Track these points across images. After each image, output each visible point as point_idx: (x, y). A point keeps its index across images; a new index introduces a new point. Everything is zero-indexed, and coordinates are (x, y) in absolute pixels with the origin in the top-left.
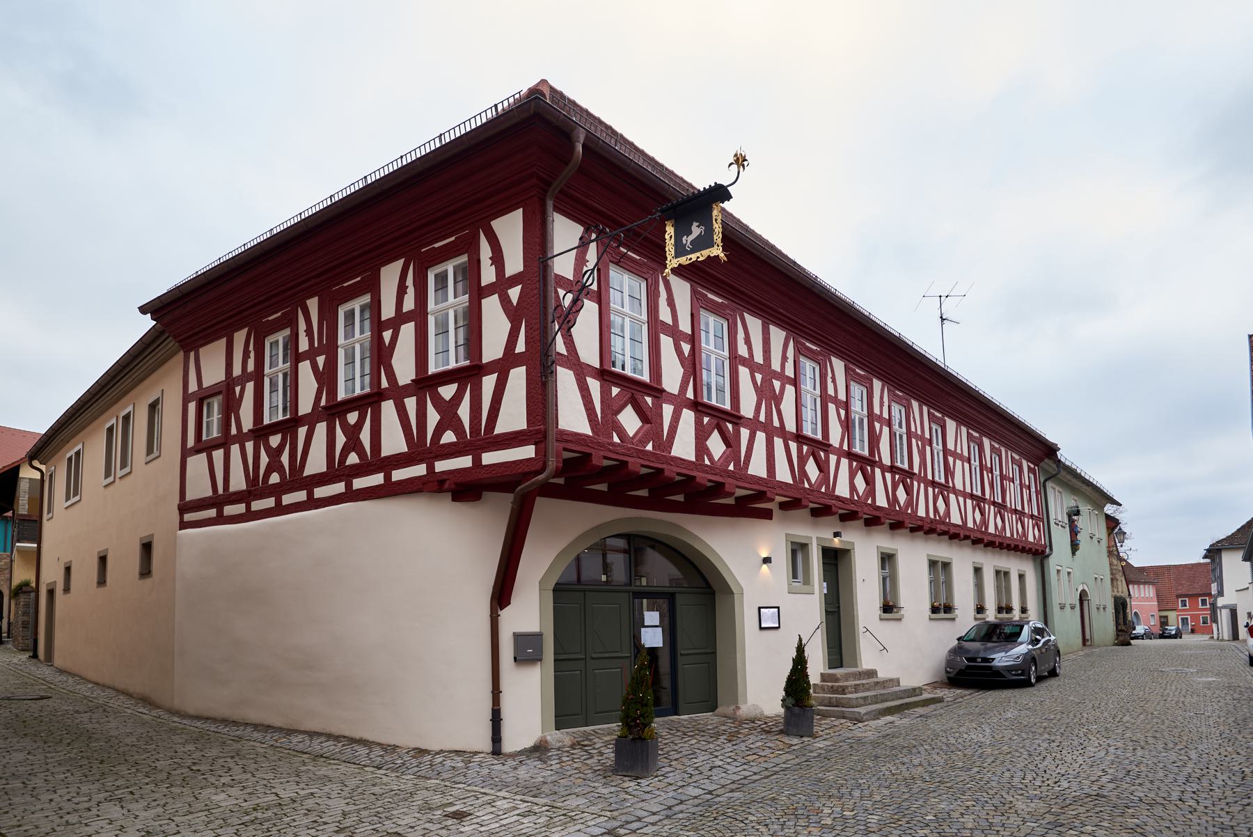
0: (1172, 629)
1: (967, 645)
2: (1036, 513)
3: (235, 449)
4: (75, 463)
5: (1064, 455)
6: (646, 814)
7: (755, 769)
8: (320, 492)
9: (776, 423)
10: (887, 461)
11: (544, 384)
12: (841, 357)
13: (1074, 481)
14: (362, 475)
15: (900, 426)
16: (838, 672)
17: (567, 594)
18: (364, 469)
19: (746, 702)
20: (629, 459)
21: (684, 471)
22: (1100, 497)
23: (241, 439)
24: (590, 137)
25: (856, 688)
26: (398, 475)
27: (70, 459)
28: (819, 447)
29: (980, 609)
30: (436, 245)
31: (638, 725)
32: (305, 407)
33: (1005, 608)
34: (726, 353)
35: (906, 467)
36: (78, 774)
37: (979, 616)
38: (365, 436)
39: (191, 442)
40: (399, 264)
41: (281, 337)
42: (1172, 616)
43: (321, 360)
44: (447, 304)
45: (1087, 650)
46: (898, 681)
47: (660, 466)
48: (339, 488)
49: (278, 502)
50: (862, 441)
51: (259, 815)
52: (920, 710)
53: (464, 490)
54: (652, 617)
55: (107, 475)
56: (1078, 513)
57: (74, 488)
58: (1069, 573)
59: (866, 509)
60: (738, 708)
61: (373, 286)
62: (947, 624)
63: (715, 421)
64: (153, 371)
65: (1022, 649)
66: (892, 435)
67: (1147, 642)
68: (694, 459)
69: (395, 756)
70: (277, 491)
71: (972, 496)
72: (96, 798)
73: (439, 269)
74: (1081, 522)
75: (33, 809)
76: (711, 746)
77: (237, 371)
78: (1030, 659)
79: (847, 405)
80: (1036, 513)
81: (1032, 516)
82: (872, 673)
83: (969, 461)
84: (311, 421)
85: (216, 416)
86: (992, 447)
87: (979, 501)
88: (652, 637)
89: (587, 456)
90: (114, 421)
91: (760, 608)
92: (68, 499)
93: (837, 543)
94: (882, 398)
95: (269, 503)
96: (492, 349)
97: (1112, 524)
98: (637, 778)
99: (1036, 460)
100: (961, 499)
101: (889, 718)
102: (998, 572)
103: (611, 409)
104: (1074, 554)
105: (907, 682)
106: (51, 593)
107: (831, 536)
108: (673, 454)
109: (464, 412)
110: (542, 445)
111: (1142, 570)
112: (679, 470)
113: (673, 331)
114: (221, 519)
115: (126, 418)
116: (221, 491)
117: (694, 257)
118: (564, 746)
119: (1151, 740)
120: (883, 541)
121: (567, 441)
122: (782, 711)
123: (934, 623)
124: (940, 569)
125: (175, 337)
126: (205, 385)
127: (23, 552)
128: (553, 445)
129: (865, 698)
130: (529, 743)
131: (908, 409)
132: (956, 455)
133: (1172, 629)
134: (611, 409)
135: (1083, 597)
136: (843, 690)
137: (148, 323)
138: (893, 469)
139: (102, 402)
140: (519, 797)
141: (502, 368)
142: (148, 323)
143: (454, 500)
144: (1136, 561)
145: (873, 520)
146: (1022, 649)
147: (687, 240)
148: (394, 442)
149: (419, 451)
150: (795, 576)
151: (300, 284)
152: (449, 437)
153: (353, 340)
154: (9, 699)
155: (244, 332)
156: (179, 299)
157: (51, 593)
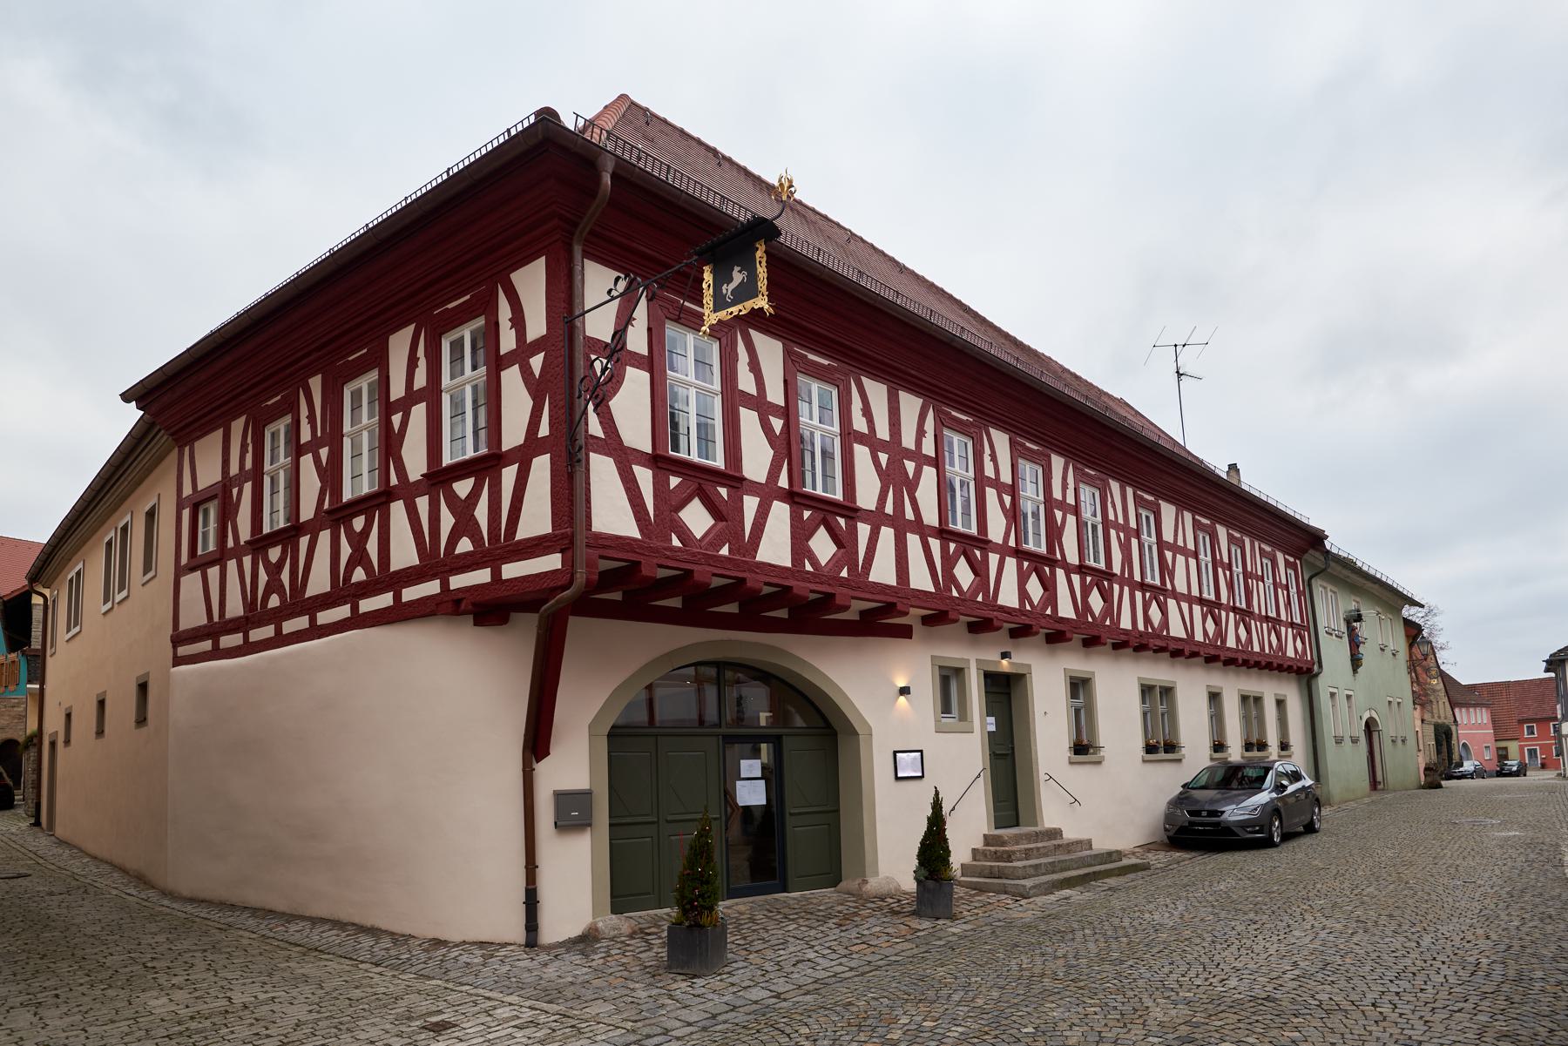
0: (1513, 764)
1: (1197, 794)
2: (1298, 621)
3: (232, 565)
4: (77, 583)
5: (1335, 543)
6: (678, 1024)
7: (853, 964)
8: (325, 617)
9: (909, 515)
10: (1073, 558)
11: (571, 476)
13: (1354, 577)
16: (1006, 833)
17: (623, 741)
18: (368, 589)
19: (877, 873)
22: (1392, 598)
23: (237, 553)
25: (1028, 854)
26: (410, 594)
28: (973, 546)
29: (1219, 747)
30: (450, 306)
31: (694, 908)
32: (307, 512)
34: (836, 429)
35: (1102, 566)
37: (1217, 755)
38: (372, 547)
39: (184, 560)
41: (281, 425)
42: (1513, 747)
43: (324, 452)
44: (462, 380)
45: (1376, 796)
46: (1089, 843)
48: (343, 612)
49: (278, 630)
50: (1037, 534)
51: (193, 1025)
52: (1112, 881)
53: (488, 610)
56: (1359, 618)
57: (75, 618)
58: (1349, 697)
59: (1043, 622)
60: (865, 882)
61: (380, 360)
62: (1169, 769)
64: (149, 471)
65: (1263, 797)
66: (1081, 525)
67: (1478, 782)
69: (403, 949)
70: (277, 616)
71: (1201, 601)
73: (453, 335)
74: (1364, 630)
76: (813, 933)
77: (234, 469)
79: (1013, 490)
80: (1298, 621)
81: (1292, 625)
82: (1055, 833)
83: (1196, 555)
84: (313, 528)
85: (212, 525)
86: (1231, 539)
88: (751, 794)
89: (636, 565)
91: (895, 753)
92: (68, 630)
94: (1064, 478)
95: (268, 631)
97: (1413, 632)
98: (695, 976)
99: (1298, 553)
100: (1185, 606)
101: (1066, 892)
102: (1244, 699)
103: (670, 504)
104: (1355, 671)
105: (1101, 845)
106: (53, 744)
107: (995, 656)
109: (481, 513)
110: (569, 554)
111: (1472, 688)
112: (767, 580)
113: (759, 403)
114: (217, 653)
115: (125, 529)
116: (216, 618)
117: (735, 310)
118: (621, 935)
119: (1383, 920)
120: (1075, 662)
121: (604, 547)
122: (910, 885)
123: (1150, 767)
124: (1157, 697)
125: (167, 428)
126: (200, 487)
128: (581, 552)
129: (1036, 867)
130: (575, 930)
132: (1175, 548)
133: (1513, 764)
134: (670, 504)
135: (1370, 727)
136: (1009, 857)
137: (132, 414)
138: (1082, 569)
139: (100, 510)
140: (528, 1003)
141: (523, 456)
142: (132, 414)
143: (478, 622)
144: (1465, 676)
145: (1058, 636)
146: (1263, 797)
147: (728, 289)
148: (404, 554)
149: (434, 564)
150: (946, 709)
151: (309, 354)
152: (465, 545)
153: (360, 426)
155: (242, 420)
157: (53, 744)
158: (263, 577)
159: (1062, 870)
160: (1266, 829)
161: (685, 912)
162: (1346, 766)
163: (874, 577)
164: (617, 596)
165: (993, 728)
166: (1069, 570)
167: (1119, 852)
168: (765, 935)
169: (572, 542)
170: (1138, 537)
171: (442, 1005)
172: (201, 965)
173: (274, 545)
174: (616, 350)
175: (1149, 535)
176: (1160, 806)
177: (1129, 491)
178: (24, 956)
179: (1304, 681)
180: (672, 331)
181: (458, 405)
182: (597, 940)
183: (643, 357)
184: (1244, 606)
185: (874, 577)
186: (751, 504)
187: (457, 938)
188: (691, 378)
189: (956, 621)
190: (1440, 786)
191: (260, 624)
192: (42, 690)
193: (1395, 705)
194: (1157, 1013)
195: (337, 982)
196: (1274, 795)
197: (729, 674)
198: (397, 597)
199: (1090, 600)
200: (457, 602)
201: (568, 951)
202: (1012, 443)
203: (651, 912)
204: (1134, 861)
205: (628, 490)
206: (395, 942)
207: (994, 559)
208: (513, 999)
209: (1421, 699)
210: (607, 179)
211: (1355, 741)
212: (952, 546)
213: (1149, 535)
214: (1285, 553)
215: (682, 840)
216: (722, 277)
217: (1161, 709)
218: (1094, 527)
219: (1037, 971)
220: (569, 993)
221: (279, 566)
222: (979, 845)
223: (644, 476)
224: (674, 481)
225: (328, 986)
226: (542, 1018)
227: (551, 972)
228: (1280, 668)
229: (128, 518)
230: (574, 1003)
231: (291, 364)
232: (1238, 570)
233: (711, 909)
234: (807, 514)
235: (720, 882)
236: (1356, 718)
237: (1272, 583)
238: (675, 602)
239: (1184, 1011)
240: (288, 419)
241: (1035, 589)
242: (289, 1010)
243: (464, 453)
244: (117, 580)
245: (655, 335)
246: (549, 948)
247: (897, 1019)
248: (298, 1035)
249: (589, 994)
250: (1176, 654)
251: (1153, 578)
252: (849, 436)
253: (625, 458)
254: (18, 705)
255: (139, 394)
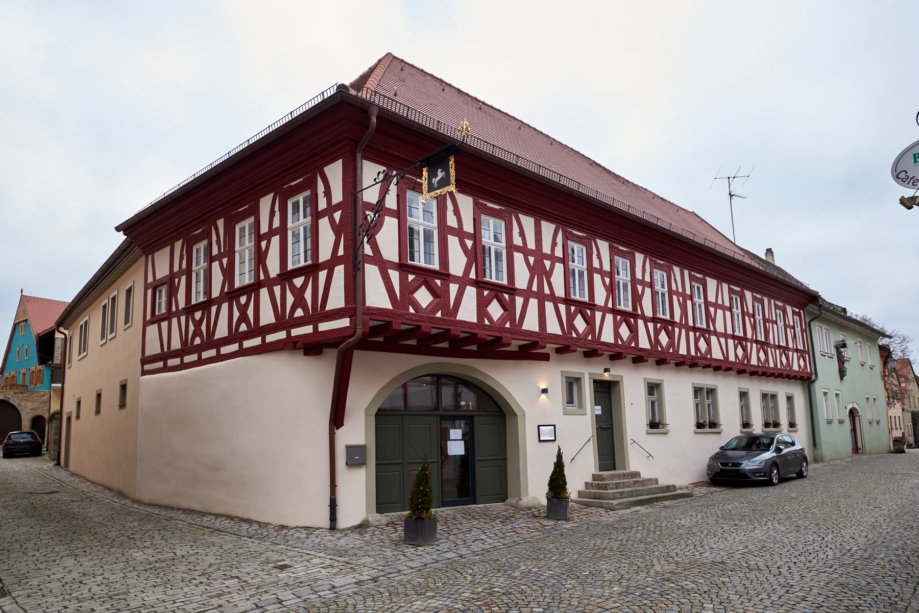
4: (85, 328)
7: (505, 542)
8: (225, 350)
10: (649, 313)
11: (355, 277)
12: (605, 238)
14: (249, 339)
15: (663, 287)
17: (383, 418)
20: (422, 324)
21: (468, 330)
22: (867, 332)
23: (178, 314)
24: (382, 110)
25: (617, 486)
26: (270, 338)
27: (81, 326)
28: (586, 308)
29: (746, 425)
31: (419, 509)
32: (216, 293)
33: (772, 424)
36: (56, 540)
38: (250, 312)
39: (148, 317)
40: (271, 196)
41: (202, 245)
43: (225, 261)
44: (298, 223)
45: (856, 457)
46: (656, 481)
47: (448, 327)
48: (234, 347)
49: (200, 357)
51: (157, 565)
52: (666, 503)
53: (312, 347)
54: (456, 434)
55: (102, 338)
56: (844, 346)
57: (83, 347)
58: (837, 395)
60: (520, 499)
63: (494, 293)
65: (768, 455)
66: (654, 294)
68: (475, 321)
69: (264, 530)
70: (199, 349)
71: (734, 337)
72: (62, 554)
73: (294, 199)
75: (21, 560)
76: (487, 526)
78: (773, 463)
81: (797, 350)
82: (637, 474)
83: (730, 309)
84: (219, 302)
85: (164, 299)
86: (754, 299)
87: (741, 341)
88: (456, 448)
89: (390, 323)
90: (106, 301)
92: (80, 354)
93: (607, 377)
95: (193, 357)
96: (325, 255)
97: (886, 353)
99: (802, 306)
100: (723, 340)
102: (764, 396)
103: (408, 290)
104: (842, 378)
106: (69, 419)
107: (602, 371)
108: (458, 318)
109: (308, 295)
110: (353, 318)
112: (463, 330)
113: (459, 233)
114: (166, 369)
115: (114, 299)
116: (166, 350)
117: (438, 191)
120: (652, 374)
121: (372, 314)
122: (544, 502)
127: (55, 389)
128: (360, 317)
129: (621, 493)
130: (357, 522)
131: (743, 298)
132: (716, 306)
135: (853, 413)
136: (605, 487)
137: (121, 237)
138: (655, 320)
141: (330, 266)
142: (121, 237)
143: (307, 353)
145: (639, 358)
146: (768, 455)
147: (435, 181)
148: (267, 317)
149: (283, 322)
150: (570, 401)
152: (299, 313)
153: (244, 247)
154: (31, 493)
156: (184, 194)
157: (69, 419)
158: (192, 328)
159: (637, 496)
160: (768, 474)
161: (414, 511)
162: (835, 439)
163: (525, 327)
164: (381, 339)
165: (600, 413)
166: (646, 320)
167: (674, 486)
168: (460, 527)
169: (355, 312)
170: (692, 299)
171: (284, 557)
172: (158, 537)
173: (198, 310)
174: (379, 208)
175: (699, 298)
176: (705, 460)
177: (772, 301)
178: (64, 532)
179: (806, 385)
180: (410, 194)
181: (296, 236)
182: (368, 527)
183: (394, 210)
184: (763, 339)
185: (525, 327)
186: (454, 288)
187: (294, 525)
188: (421, 220)
189: (575, 351)
190: (904, 452)
191: (189, 353)
192: (63, 387)
193: (871, 400)
194: (658, 568)
195: (230, 546)
196: (774, 454)
197: (444, 380)
198: (263, 340)
199: (660, 337)
200: (295, 343)
201: (352, 532)
202: (611, 247)
203: (399, 513)
204: (685, 491)
205: (385, 283)
206: (260, 526)
207: (598, 315)
208: (322, 555)
209: (895, 396)
210: (374, 119)
211: (841, 422)
212: (573, 308)
213: (699, 298)
214: (792, 306)
215: (413, 473)
216: (432, 174)
217: (707, 402)
218: (663, 295)
219: (603, 547)
220: (350, 553)
221: (200, 322)
222: (590, 480)
223: (394, 275)
224: (411, 277)
225: (225, 547)
226: (336, 564)
227: (342, 542)
228: (789, 377)
229: (116, 293)
230: (354, 558)
231: (208, 212)
232: (759, 317)
233: (428, 510)
234: (486, 293)
235: (435, 495)
236: (842, 408)
237: (782, 326)
238: (413, 342)
239: (673, 566)
240: (205, 242)
241: (624, 331)
242: (205, 558)
243: (299, 263)
244: (108, 328)
245: (401, 198)
246: (342, 531)
247: (520, 567)
248: (211, 570)
249: (361, 553)
250: (717, 369)
251: (701, 323)
252: (511, 248)
253: (384, 266)
254: (44, 395)
255: (126, 228)
